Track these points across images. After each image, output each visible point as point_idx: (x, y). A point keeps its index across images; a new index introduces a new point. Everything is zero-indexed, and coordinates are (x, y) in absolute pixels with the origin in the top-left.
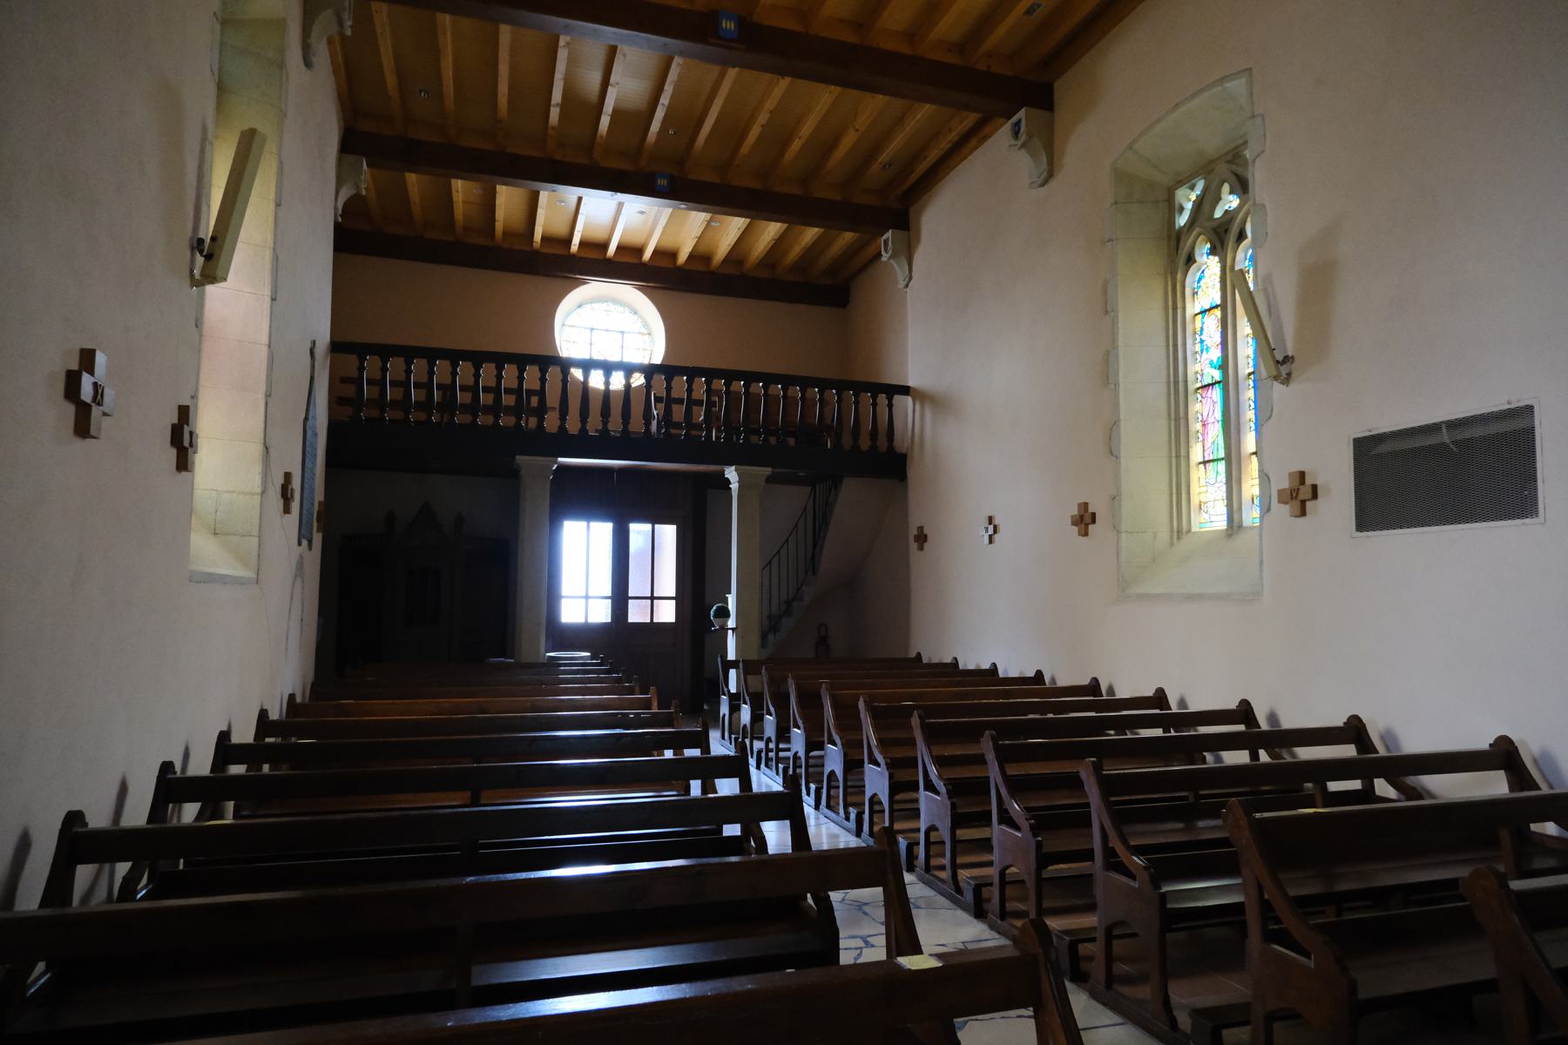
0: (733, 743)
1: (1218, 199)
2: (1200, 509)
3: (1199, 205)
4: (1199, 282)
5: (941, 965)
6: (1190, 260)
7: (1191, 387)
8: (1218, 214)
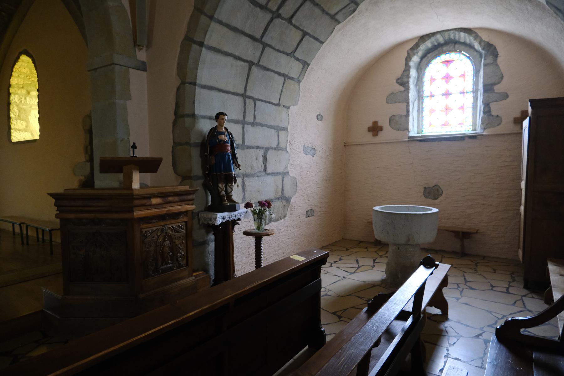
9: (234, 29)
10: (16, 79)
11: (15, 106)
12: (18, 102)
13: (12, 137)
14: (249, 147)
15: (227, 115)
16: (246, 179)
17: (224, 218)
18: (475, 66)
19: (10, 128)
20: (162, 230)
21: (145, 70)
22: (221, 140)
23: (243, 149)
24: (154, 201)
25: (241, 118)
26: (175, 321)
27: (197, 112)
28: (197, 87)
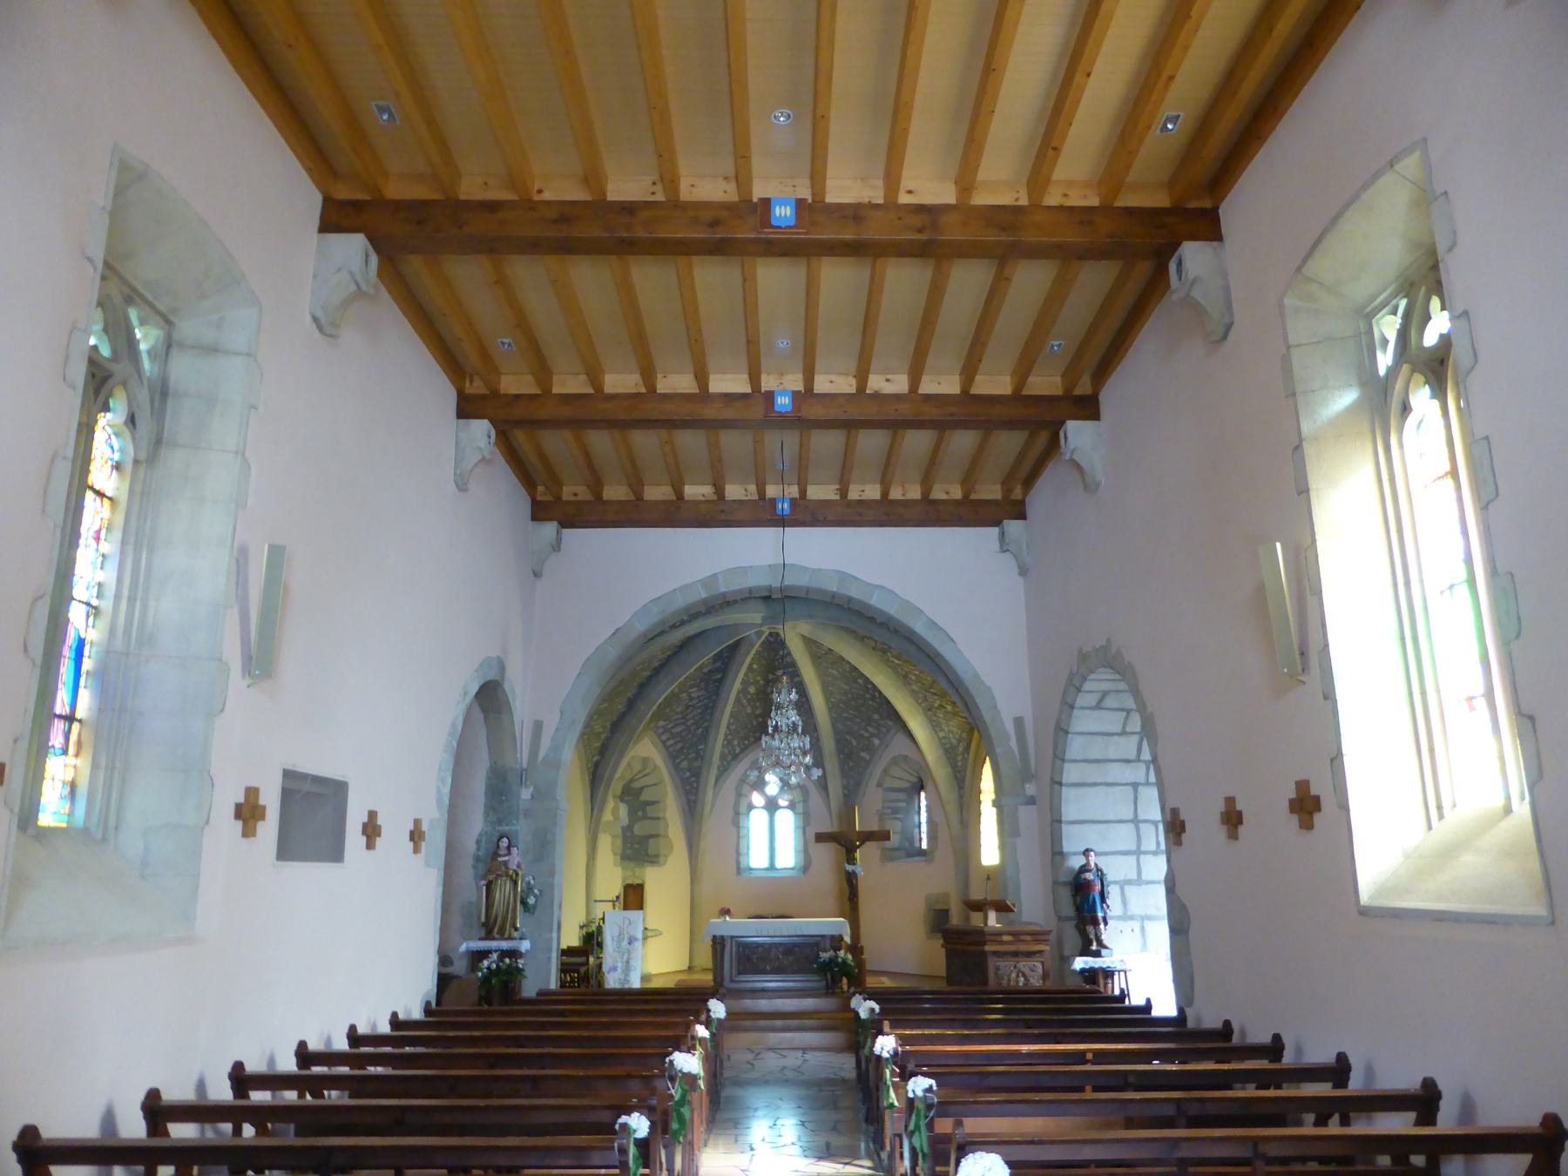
0: (71, 639)
3: (1403, 335)
6: (1406, 409)
9: (1097, 761)
11: (852, 964)
14: (1148, 883)
15: (1092, 850)
16: (1146, 922)
17: (1086, 963)
20: (1015, 967)
21: (1034, 804)
22: (1085, 879)
23: (1140, 885)
24: (1005, 938)
25: (1134, 847)
26: (984, 1006)
27: (1065, 850)
28: (1063, 825)
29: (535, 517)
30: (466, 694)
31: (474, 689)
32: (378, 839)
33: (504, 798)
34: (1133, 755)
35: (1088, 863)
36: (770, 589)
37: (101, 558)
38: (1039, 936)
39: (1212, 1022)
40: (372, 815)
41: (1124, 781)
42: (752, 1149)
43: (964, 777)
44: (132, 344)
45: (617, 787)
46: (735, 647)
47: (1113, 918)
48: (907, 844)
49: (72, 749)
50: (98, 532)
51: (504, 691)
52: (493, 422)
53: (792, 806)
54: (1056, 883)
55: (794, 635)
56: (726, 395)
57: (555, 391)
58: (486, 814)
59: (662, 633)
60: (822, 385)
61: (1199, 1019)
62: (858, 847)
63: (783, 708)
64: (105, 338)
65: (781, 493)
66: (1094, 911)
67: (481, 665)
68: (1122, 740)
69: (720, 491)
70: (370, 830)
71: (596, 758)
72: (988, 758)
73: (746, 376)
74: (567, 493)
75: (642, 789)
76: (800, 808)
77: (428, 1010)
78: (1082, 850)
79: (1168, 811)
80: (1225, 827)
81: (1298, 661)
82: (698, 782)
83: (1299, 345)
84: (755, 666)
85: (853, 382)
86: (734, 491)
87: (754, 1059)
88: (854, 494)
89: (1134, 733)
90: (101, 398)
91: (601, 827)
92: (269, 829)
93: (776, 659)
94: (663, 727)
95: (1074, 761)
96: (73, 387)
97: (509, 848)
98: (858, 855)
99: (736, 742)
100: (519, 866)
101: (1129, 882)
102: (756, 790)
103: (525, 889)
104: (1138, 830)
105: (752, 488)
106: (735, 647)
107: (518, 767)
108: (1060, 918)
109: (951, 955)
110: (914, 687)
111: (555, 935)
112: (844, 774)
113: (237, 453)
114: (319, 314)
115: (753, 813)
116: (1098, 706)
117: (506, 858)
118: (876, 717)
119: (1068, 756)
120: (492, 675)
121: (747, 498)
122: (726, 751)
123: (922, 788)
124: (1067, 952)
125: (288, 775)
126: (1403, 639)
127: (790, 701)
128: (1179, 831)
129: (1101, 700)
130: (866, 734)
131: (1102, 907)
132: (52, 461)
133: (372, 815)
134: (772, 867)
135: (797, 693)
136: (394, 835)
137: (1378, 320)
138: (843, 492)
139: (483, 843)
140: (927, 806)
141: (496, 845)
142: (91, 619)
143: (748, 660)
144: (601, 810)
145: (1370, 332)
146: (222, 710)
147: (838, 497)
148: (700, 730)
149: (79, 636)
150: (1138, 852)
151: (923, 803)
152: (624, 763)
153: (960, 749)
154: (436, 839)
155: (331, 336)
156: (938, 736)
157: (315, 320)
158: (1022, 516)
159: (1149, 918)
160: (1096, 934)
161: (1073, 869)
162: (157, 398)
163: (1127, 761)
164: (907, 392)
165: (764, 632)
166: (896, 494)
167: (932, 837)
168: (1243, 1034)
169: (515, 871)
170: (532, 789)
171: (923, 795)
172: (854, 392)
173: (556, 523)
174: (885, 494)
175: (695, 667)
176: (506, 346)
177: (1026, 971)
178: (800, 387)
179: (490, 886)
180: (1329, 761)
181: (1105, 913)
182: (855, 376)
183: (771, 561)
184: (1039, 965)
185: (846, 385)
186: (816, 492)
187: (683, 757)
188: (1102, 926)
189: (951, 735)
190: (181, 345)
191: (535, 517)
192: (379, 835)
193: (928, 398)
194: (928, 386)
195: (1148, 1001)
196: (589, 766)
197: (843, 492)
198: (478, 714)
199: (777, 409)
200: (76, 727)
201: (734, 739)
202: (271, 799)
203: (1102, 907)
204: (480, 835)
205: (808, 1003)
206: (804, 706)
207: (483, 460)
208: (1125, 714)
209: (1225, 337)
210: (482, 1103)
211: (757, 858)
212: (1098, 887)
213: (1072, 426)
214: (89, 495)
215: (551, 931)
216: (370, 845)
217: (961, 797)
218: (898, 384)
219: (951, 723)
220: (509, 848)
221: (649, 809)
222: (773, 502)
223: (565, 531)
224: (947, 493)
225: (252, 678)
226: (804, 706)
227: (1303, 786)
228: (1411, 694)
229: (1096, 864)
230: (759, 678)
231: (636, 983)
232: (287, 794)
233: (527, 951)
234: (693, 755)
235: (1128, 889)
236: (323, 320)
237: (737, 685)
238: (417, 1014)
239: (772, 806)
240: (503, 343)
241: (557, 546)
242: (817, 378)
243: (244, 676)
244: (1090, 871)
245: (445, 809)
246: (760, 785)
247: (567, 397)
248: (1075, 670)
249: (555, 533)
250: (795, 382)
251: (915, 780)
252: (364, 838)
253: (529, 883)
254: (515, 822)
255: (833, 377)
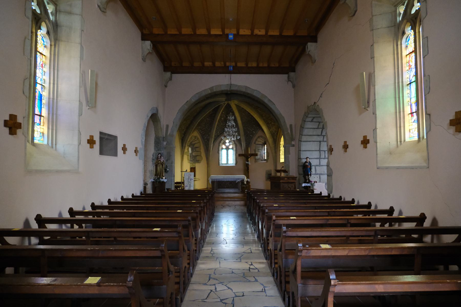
0: (37, 94)
1: (413, 5)
2: (410, 132)
3: (405, 11)
4: (408, 42)
5: (320, 245)
6: (404, 33)
7: (405, 84)
8: (413, 12)
9: (311, 135)
10: (282, 142)
12: (214, 191)
13: (280, 161)
16: (321, 175)
17: (305, 185)
18: (122, 209)
19: (280, 158)
22: (306, 165)
24: (285, 179)
25: (319, 157)
27: (301, 157)
29: (165, 71)
30: (148, 116)
31: (150, 115)
32: (126, 151)
33: (159, 144)
34: (320, 134)
35: (307, 161)
36: (227, 90)
37: (44, 72)
38: (294, 178)
39: (337, 196)
40: (124, 145)
41: (317, 141)
42: (222, 226)
43: (276, 141)
44: (46, 10)
45: (188, 143)
46: (219, 106)
47: (313, 174)
48: (261, 158)
49: (42, 124)
50: (42, 65)
51: (158, 117)
52: (151, 42)
53: (232, 149)
54: (298, 166)
55: (233, 104)
56: (215, 35)
57: (168, 33)
58: (155, 149)
59: (199, 103)
60: (242, 32)
61: (333, 196)
62: (249, 157)
63: (230, 121)
64: (38, 7)
65: (230, 65)
66: (308, 172)
67: (152, 109)
68: (318, 130)
69: (214, 64)
70: (124, 149)
71: (183, 136)
72: (282, 136)
73: (220, 29)
74: (173, 64)
75: (195, 144)
76: (235, 149)
77: (141, 193)
78: (306, 157)
79: (329, 146)
80: (343, 149)
81: (367, 104)
82: (209, 142)
83: (376, 15)
84: (223, 113)
85: (250, 31)
86: (218, 64)
87: (223, 207)
88: (250, 65)
89: (321, 128)
90: (38, 24)
91: (184, 153)
92: (97, 146)
93: (229, 110)
94: (200, 128)
95: (305, 135)
96: (28, 18)
97: (161, 157)
98: (249, 159)
99: (218, 132)
100: (163, 161)
101: (317, 166)
102: (223, 144)
103: (165, 167)
104: (320, 153)
105: (222, 63)
106: (218, 108)
107: (162, 136)
108: (299, 174)
109: (272, 184)
110: (264, 118)
111: (173, 178)
112: (246, 141)
113: (79, 44)
114: (99, 4)
115: (223, 150)
116: (312, 121)
117: (160, 159)
118: (254, 126)
119: (304, 127)
120: (155, 112)
121: (221, 66)
122: (216, 134)
123: (265, 144)
124: (301, 182)
125: (101, 133)
126: (396, 98)
127: (232, 119)
128: (331, 151)
129: (312, 120)
130: (252, 130)
131: (310, 172)
132: (25, 41)
133: (124, 145)
134: (227, 163)
135: (234, 117)
136: (131, 150)
137: (399, 7)
138: (247, 64)
139: (154, 156)
140: (266, 148)
141: (157, 156)
142: (43, 89)
143: (221, 111)
144: (184, 149)
145: (396, 11)
146: (82, 115)
147: (245, 66)
148: (209, 129)
149: (40, 94)
150: (320, 158)
151: (266, 147)
152: (190, 137)
153: (276, 134)
154: (141, 152)
155: (103, 12)
156: (270, 131)
157: (99, 6)
158: (294, 71)
159: (322, 174)
160: (308, 178)
161: (303, 162)
162: (55, 27)
163: (318, 135)
164: (264, 34)
165: (226, 103)
166: (261, 65)
167: (267, 156)
168: (344, 199)
169: (163, 162)
170: (166, 142)
171: (266, 145)
172: (250, 34)
173: (170, 72)
174: (258, 64)
175: (208, 113)
176: (154, 19)
177: (290, 187)
178: (235, 32)
179: (156, 166)
180: (373, 130)
181: (311, 173)
182: (251, 30)
183: (228, 83)
184: (293, 185)
185: (248, 32)
186: (239, 65)
187: (205, 136)
188: (310, 176)
189: (273, 130)
190: (60, 11)
191: (165, 71)
192: (127, 150)
193: (271, 36)
194: (271, 33)
195: (321, 192)
196: (181, 138)
197: (247, 64)
198: (151, 122)
199: (229, 39)
200: (42, 118)
201: (218, 132)
202: (97, 138)
203: (310, 172)
204: (153, 153)
205: (236, 195)
206: (235, 120)
207: (149, 53)
208: (318, 123)
209: (354, 15)
210: (154, 211)
211: (223, 161)
212: (309, 167)
213: (309, 44)
214: (38, 54)
215: (172, 177)
216: (124, 153)
217: (275, 146)
218: (262, 32)
219: (274, 127)
220: (161, 157)
221: (197, 149)
222: (228, 67)
223: (173, 75)
224: (275, 65)
225: (89, 107)
226: (235, 120)
227: (365, 137)
228: (396, 112)
229: (309, 161)
230: (224, 116)
231: (192, 189)
232: (101, 139)
233: (166, 182)
234: (207, 135)
235: (317, 167)
236: (101, 7)
237: (218, 118)
238: (139, 194)
239: (227, 148)
240: (153, 18)
241: (171, 79)
242: (240, 30)
243: (87, 106)
244: (307, 163)
245: (144, 145)
246: (224, 143)
247: (172, 35)
248: (306, 111)
249: (170, 75)
250: (234, 31)
251: (264, 142)
252: (123, 151)
253: (166, 165)
254: (162, 150)
255: (245, 30)
